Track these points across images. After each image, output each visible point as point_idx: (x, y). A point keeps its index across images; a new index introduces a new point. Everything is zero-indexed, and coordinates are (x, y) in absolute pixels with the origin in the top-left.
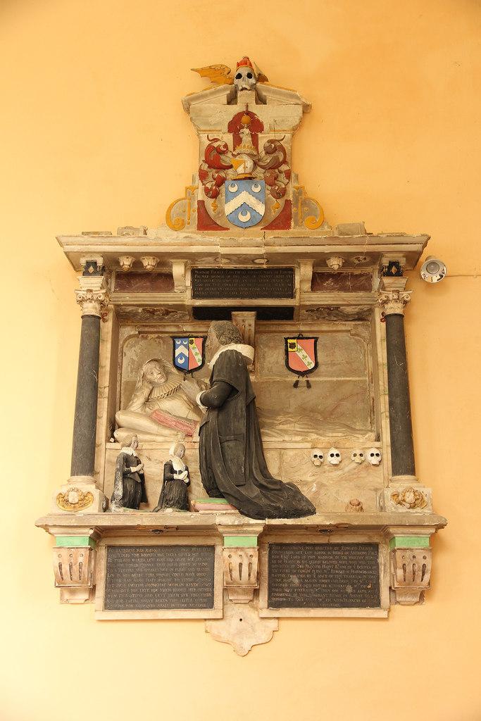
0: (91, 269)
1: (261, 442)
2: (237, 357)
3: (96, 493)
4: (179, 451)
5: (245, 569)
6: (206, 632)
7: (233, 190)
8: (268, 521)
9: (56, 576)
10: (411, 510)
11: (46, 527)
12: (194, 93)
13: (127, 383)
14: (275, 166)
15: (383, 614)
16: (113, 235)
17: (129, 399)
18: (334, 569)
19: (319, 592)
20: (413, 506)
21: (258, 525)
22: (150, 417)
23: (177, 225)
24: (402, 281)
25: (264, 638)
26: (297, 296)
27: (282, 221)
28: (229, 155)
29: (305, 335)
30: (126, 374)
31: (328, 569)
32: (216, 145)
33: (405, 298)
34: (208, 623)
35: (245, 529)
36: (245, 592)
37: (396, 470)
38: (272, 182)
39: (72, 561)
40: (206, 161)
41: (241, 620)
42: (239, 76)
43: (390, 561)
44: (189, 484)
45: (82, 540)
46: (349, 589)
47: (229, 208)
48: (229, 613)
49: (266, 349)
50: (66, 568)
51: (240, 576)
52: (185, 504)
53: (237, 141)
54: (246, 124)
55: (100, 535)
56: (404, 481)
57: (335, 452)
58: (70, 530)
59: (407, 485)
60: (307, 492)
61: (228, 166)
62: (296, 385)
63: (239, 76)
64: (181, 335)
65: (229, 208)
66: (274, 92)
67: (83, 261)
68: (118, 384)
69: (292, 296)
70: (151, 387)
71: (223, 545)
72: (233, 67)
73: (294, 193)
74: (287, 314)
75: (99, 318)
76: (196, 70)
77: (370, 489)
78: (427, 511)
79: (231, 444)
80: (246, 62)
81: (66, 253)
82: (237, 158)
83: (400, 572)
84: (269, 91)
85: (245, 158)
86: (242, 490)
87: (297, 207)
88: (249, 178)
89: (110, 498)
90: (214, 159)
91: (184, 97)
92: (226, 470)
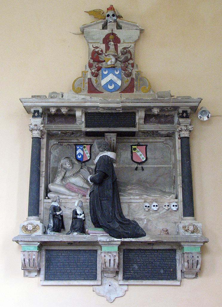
0: (36, 114)
1: (119, 199)
2: (108, 160)
3: (41, 225)
4: (80, 204)
5: (112, 262)
6: (93, 291)
7: (106, 73)
8: (123, 240)
9: (22, 264)
10: (192, 234)
11: (17, 242)
12: (86, 24)
13: (53, 168)
14: (127, 61)
15: (178, 283)
16: (48, 98)
17: (54, 177)
18: (155, 261)
19: (148, 273)
20: (193, 232)
21: (118, 241)
22: (65, 186)
23: (77, 90)
24: (189, 121)
25: (121, 294)
26: (137, 126)
27: (130, 89)
28: (104, 55)
29: (141, 144)
30: (52, 164)
31: (150, 262)
32: (97, 50)
33: (190, 129)
34: (94, 287)
35: (112, 243)
36: (112, 272)
37: (185, 215)
38: (125, 69)
39: (30, 258)
40: (92, 58)
41: (110, 285)
42: (108, 16)
43: (182, 258)
44: (84, 220)
45: (34, 248)
46: (162, 271)
47: (104, 82)
48: (104, 282)
49: (122, 151)
50: (27, 261)
51: (110, 266)
52: (82, 230)
53: (108, 48)
54: (112, 39)
55: (42, 245)
56: (189, 220)
57: (155, 204)
58: (28, 243)
59: (190, 222)
60: (141, 224)
61: (103, 61)
62: (136, 169)
63: (108, 16)
64: (79, 143)
65: (104, 82)
66: (125, 23)
67: (32, 110)
68: (49, 168)
69: (134, 126)
70: (65, 171)
71: (101, 251)
72: (105, 10)
73: (136, 74)
74: (132, 134)
75: (40, 138)
76: (87, 12)
77: (173, 223)
78: (199, 235)
79: (105, 202)
80: (111, 8)
81: (24, 106)
82: (107, 57)
83: (186, 264)
84: (122, 23)
85: (112, 57)
86: (110, 224)
87: (137, 81)
88: (113, 67)
89: (47, 227)
90: (96, 58)
91: (81, 26)
92: (103, 215)
